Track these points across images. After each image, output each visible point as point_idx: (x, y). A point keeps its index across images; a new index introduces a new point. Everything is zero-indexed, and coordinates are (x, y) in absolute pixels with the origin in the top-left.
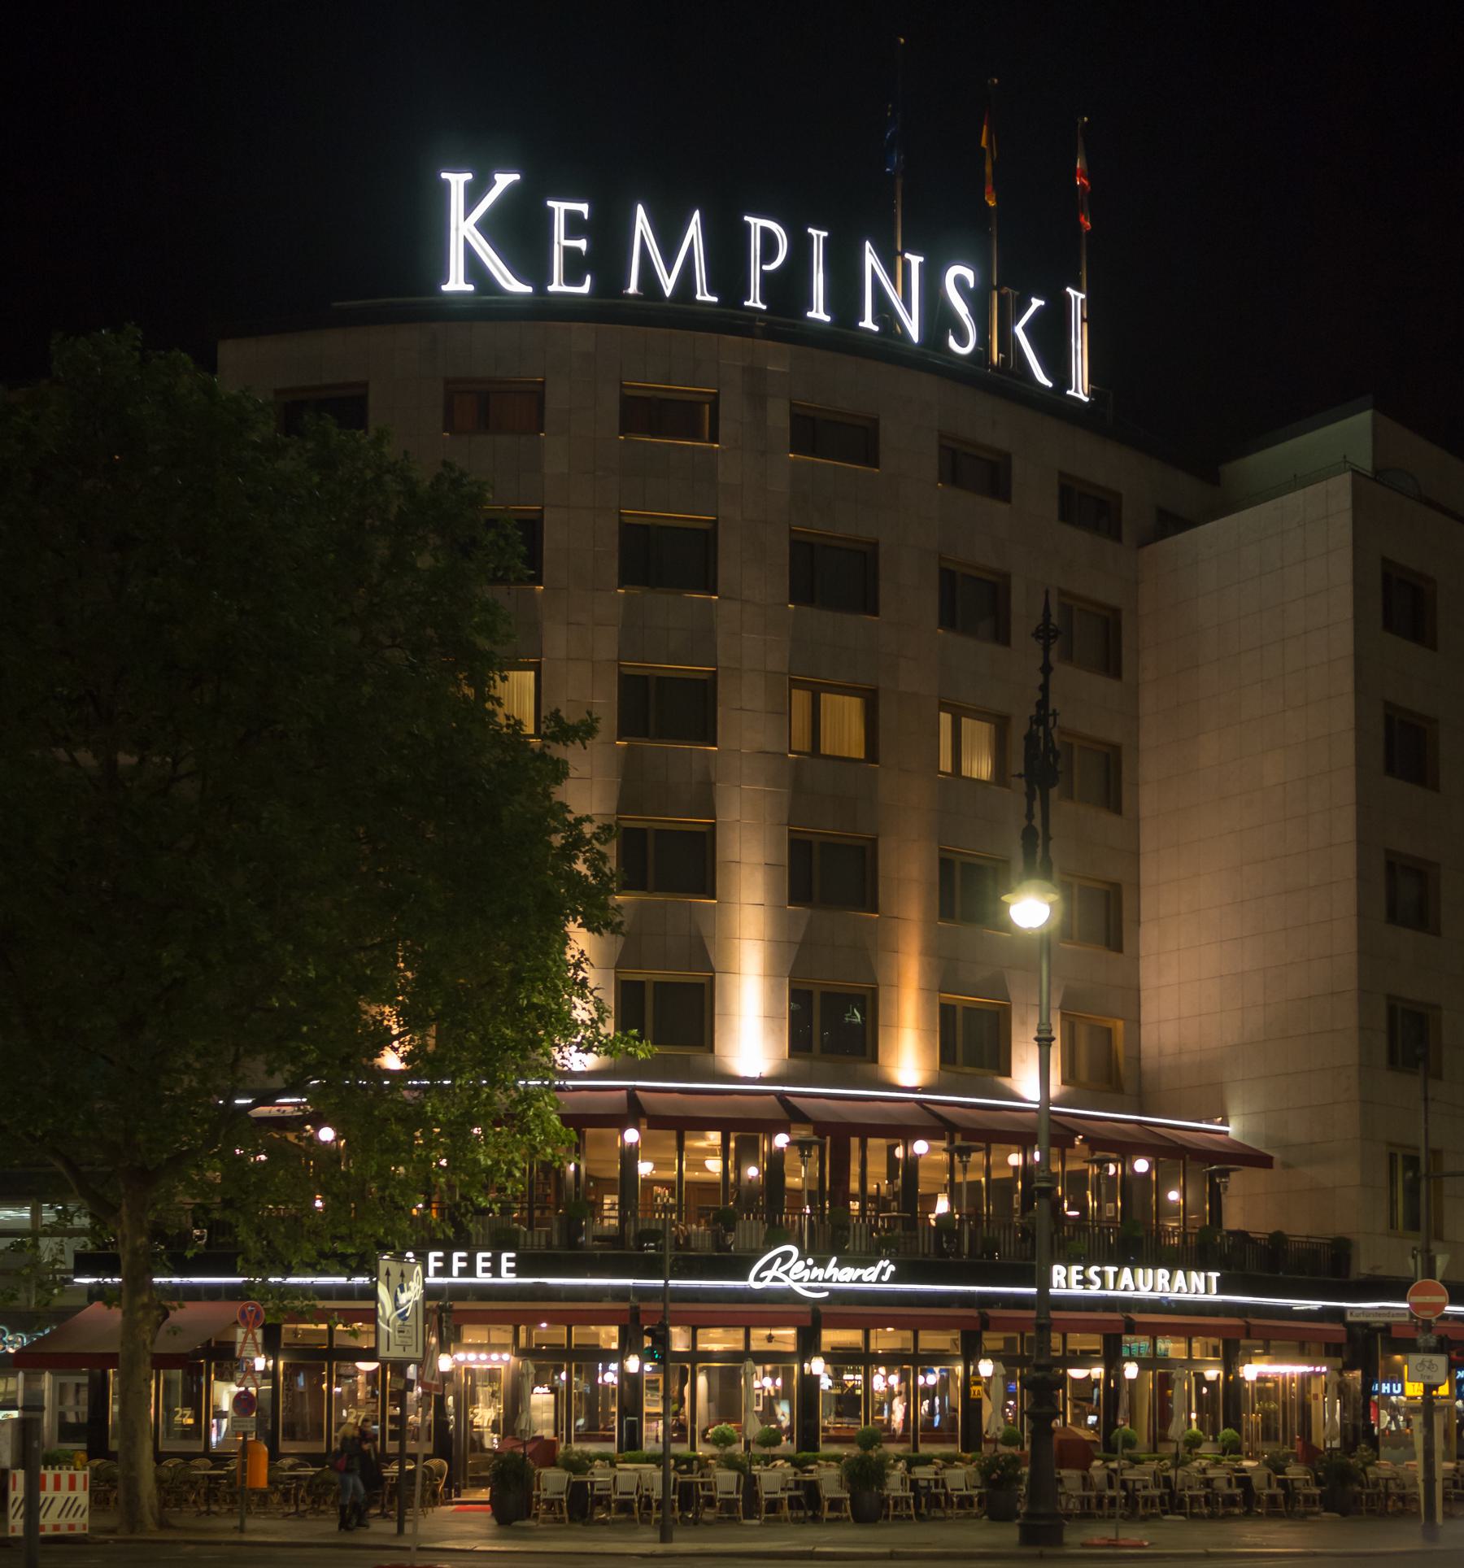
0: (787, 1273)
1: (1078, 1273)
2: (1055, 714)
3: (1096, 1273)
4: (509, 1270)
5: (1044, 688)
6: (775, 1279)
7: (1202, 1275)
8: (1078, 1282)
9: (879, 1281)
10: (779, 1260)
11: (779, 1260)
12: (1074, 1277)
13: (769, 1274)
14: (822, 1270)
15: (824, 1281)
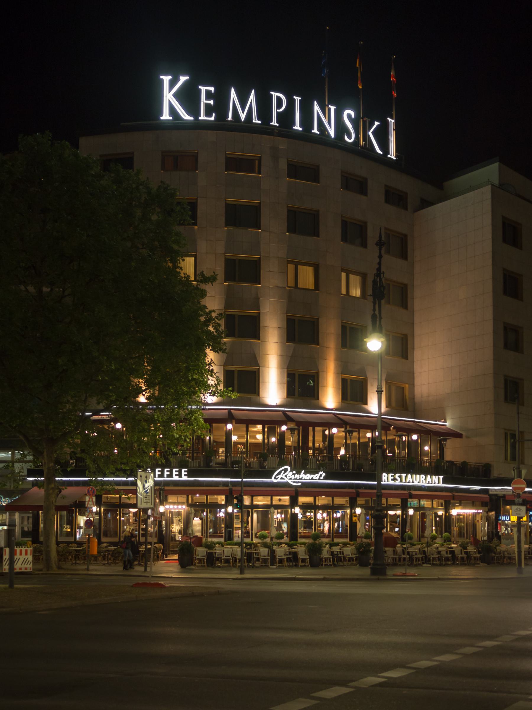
0: (286, 476)
1: (392, 476)
2: (383, 273)
3: (398, 476)
4: (185, 475)
5: (379, 264)
6: (282, 478)
7: (437, 477)
8: (392, 480)
9: (319, 479)
10: (283, 472)
11: (283, 472)
12: (390, 478)
13: (280, 477)
14: (299, 475)
15: (299, 479)
